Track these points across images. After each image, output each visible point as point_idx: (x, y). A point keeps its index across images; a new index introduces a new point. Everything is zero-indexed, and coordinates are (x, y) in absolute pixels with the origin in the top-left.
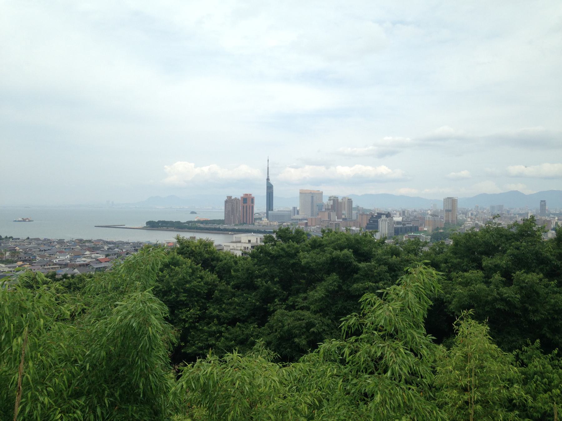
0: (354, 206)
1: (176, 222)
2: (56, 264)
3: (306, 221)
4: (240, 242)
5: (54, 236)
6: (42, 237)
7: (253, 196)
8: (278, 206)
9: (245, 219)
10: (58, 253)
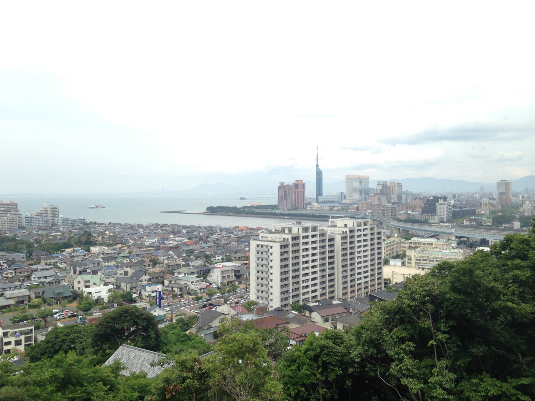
0: (404, 190)
3: (357, 206)
4: (336, 226)
5: (134, 221)
6: (123, 222)
7: (304, 182)
8: (326, 191)
9: (297, 203)
10: (145, 237)
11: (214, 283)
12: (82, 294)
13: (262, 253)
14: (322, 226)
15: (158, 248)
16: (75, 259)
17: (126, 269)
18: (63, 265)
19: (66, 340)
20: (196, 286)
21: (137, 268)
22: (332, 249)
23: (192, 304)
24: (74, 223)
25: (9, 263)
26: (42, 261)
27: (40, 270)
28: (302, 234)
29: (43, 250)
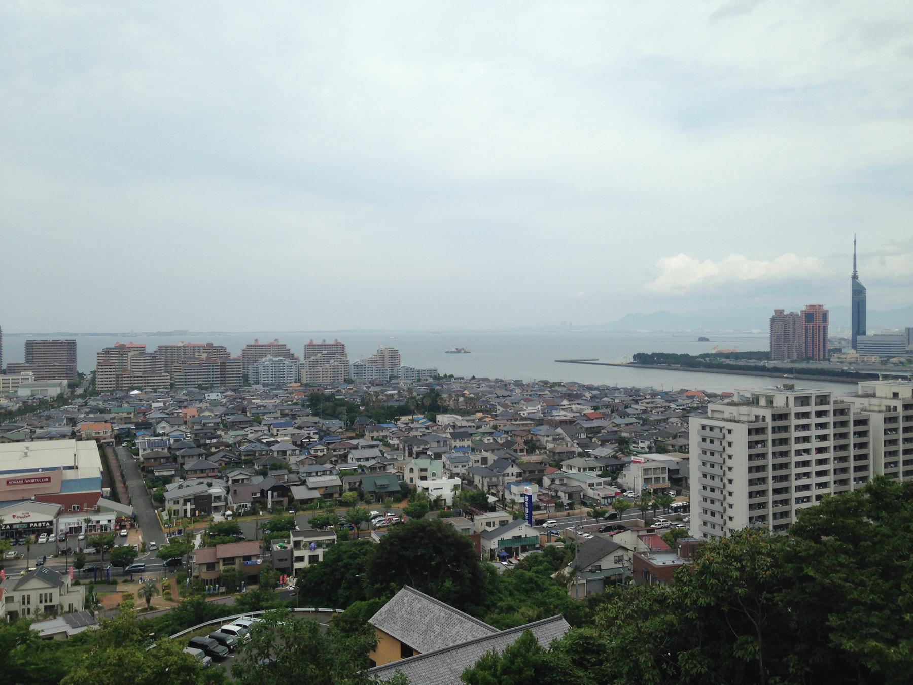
1: (681, 355)
2: (526, 419)
5: (508, 376)
6: (492, 377)
7: (825, 308)
8: (873, 328)
10: (523, 402)
11: (630, 489)
12: (415, 489)
13: (712, 442)
14: (838, 392)
15: (540, 422)
16: (413, 434)
17: (485, 454)
18: (395, 442)
19: (351, 565)
20: (596, 492)
21: (502, 453)
22: (862, 440)
23: (587, 523)
24: (419, 377)
25: (322, 434)
26: (367, 433)
27: (362, 447)
28: (795, 409)
29: (370, 417)
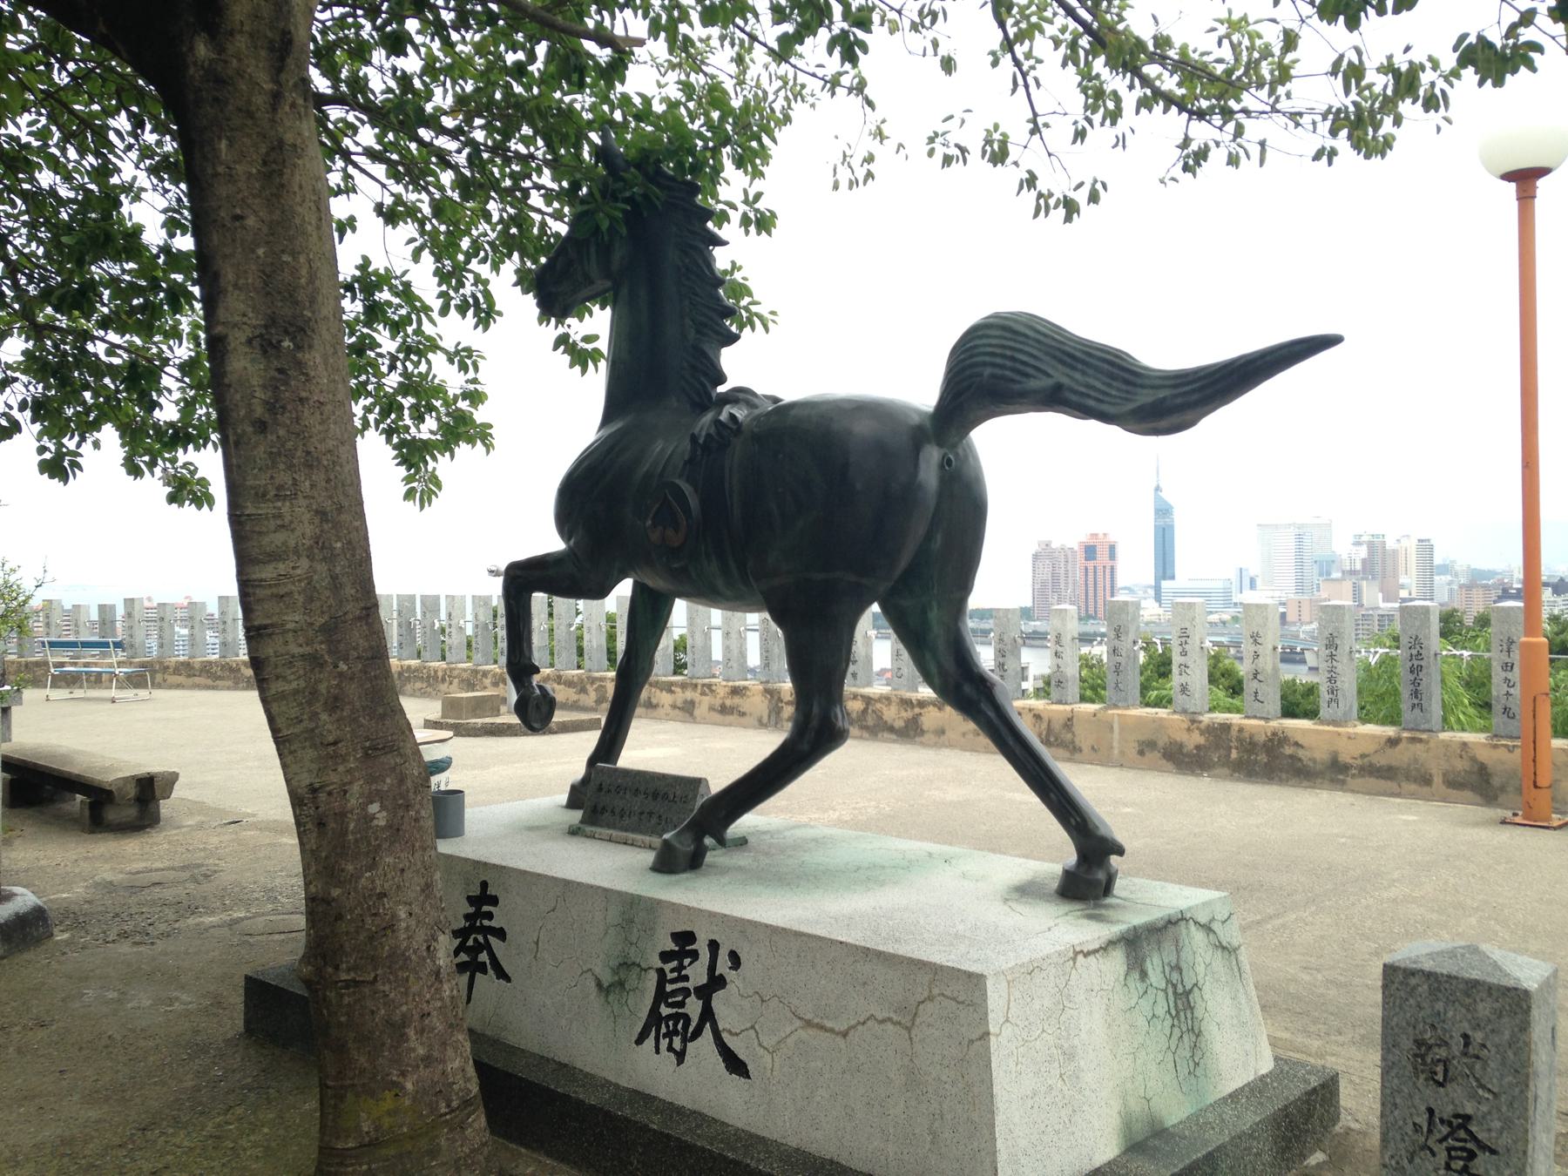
7: (1112, 538)
